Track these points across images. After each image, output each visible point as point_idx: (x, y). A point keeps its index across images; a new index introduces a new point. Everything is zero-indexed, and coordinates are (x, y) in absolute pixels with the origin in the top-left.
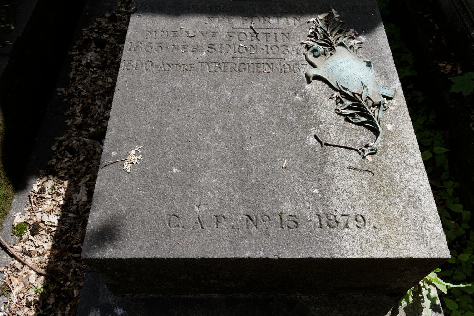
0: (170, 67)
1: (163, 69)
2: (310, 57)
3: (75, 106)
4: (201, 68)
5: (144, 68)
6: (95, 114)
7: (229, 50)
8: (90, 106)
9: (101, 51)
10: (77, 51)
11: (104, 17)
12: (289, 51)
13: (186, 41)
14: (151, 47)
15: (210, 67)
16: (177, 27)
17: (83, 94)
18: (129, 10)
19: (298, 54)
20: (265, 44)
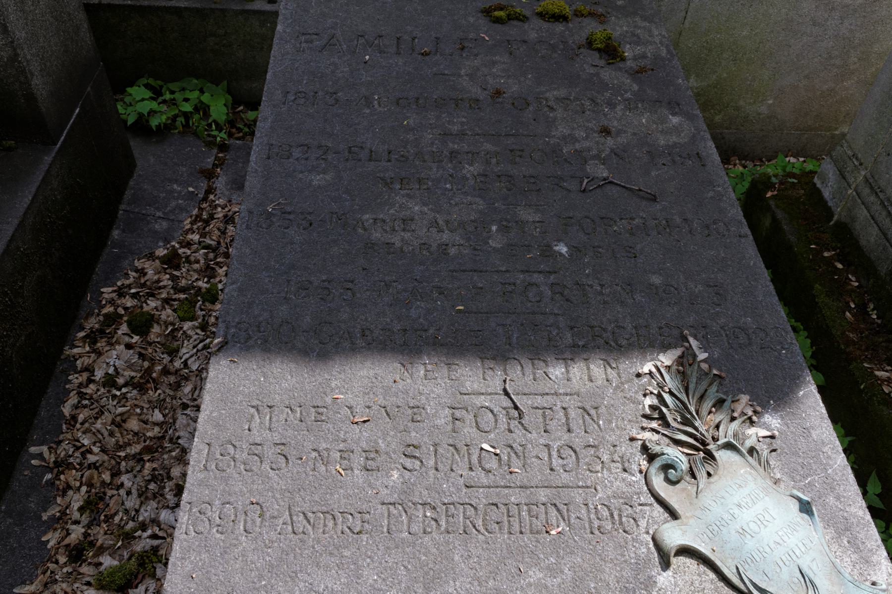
0: (309, 522)
1: (290, 528)
2: (658, 482)
3: (70, 493)
4: (389, 522)
5: (239, 528)
6: (116, 513)
7: (457, 463)
8: (107, 490)
9: (142, 342)
10: (87, 345)
11: (151, 257)
12: (602, 462)
13: (347, 435)
14: (260, 458)
15: (410, 519)
16: (325, 393)
17: (92, 458)
18: (207, 237)
19: (625, 470)
20: (542, 441)
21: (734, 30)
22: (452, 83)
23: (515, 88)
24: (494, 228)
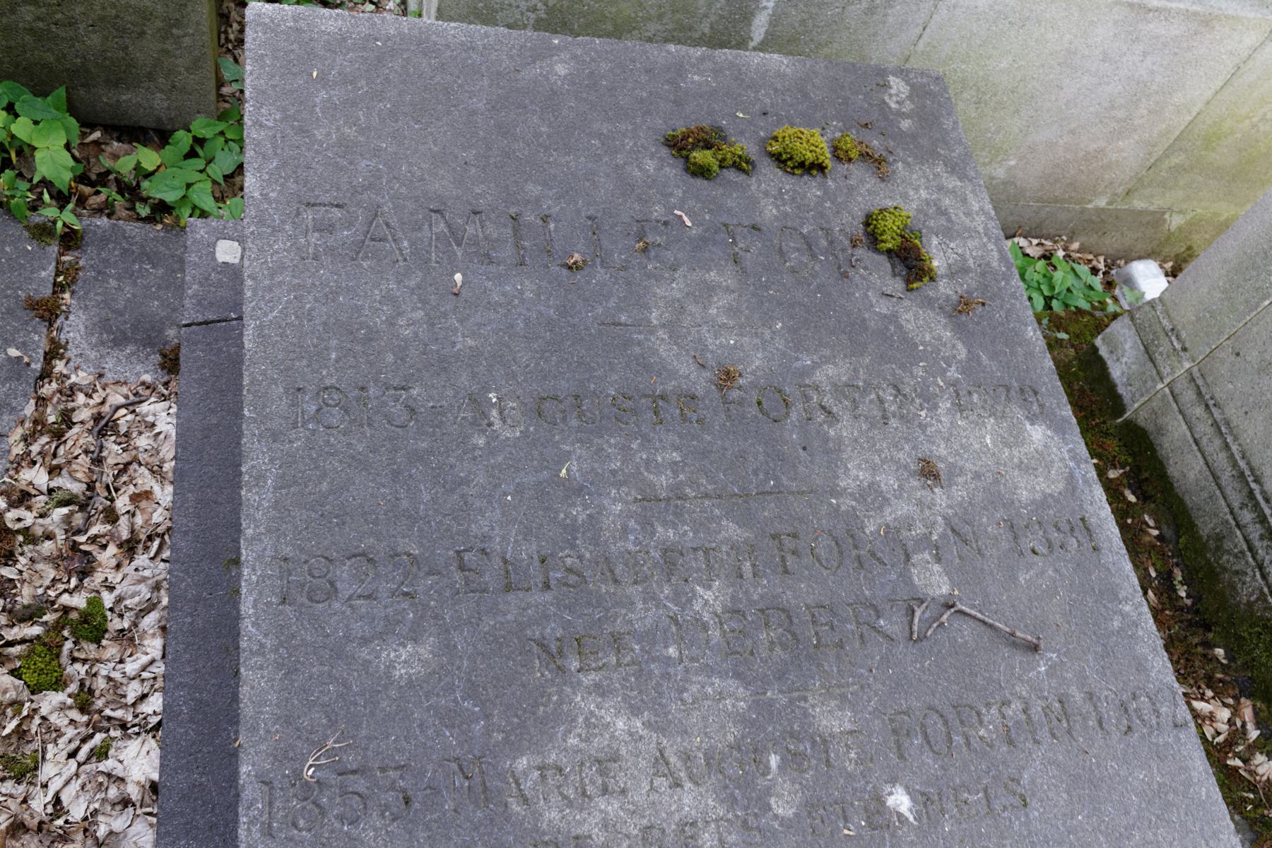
21: (989, 59)
22: (637, 350)
23: (758, 361)
24: (774, 761)
